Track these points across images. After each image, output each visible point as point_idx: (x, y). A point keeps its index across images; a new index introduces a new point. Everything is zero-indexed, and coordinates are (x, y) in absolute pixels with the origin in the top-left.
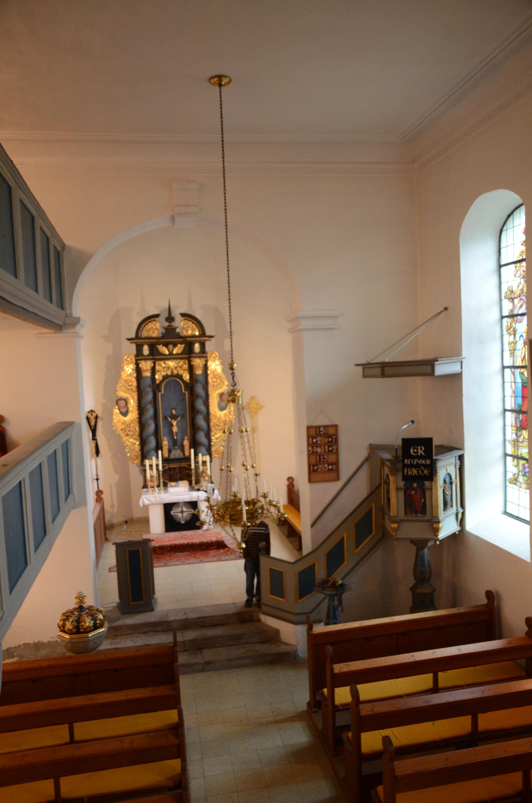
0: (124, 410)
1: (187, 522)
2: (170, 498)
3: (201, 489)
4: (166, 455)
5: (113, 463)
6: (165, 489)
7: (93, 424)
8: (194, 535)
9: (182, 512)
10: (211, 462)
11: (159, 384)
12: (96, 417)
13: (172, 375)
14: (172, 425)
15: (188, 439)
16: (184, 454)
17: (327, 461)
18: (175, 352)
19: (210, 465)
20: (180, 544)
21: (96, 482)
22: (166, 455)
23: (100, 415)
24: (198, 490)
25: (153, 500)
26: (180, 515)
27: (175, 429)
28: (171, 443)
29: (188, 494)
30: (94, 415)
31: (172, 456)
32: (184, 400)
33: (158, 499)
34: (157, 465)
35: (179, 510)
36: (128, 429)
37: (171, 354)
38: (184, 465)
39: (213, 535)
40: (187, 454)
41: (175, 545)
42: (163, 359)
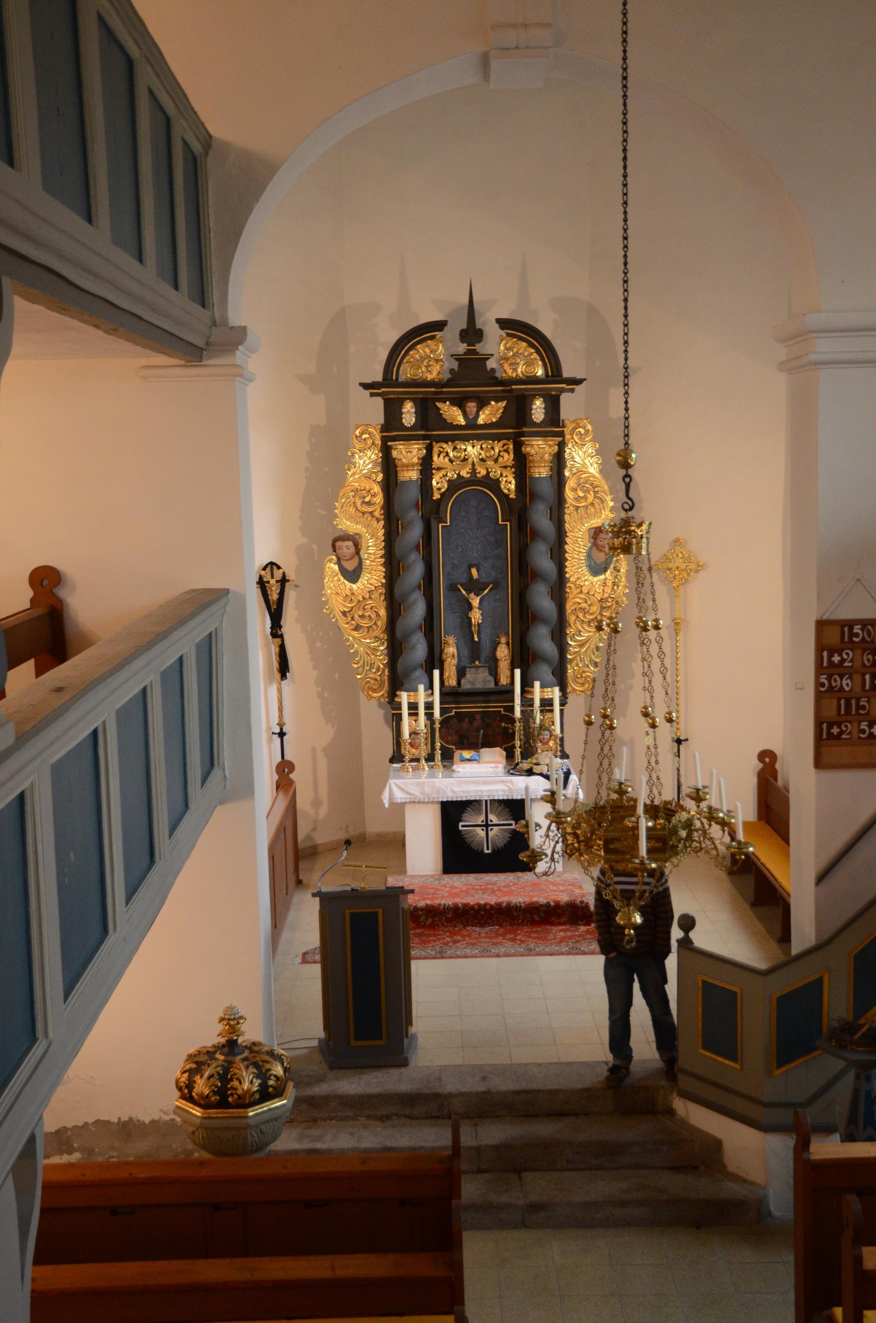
0: (350, 566)
1: (497, 852)
2: (456, 789)
3: (536, 769)
5: (320, 695)
8: (515, 884)
9: (487, 825)
10: (563, 704)
12: (283, 581)
13: (474, 480)
15: (508, 644)
16: (497, 683)
17: (868, 713)
19: (562, 711)
20: (479, 905)
21: (277, 740)
22: (452, 682)
23: (291, 575)
24: (530, 772)
25: (417, 793)
26: (481, 832)
27: (476, 616)
28: (466, 653)
29: (503, 782)
30: (278, 574)
31: (466, 685)
32: (500, 543)
33: (427, 790)
36: (360, 613)
39: (561, 888)
40: (504, 680)
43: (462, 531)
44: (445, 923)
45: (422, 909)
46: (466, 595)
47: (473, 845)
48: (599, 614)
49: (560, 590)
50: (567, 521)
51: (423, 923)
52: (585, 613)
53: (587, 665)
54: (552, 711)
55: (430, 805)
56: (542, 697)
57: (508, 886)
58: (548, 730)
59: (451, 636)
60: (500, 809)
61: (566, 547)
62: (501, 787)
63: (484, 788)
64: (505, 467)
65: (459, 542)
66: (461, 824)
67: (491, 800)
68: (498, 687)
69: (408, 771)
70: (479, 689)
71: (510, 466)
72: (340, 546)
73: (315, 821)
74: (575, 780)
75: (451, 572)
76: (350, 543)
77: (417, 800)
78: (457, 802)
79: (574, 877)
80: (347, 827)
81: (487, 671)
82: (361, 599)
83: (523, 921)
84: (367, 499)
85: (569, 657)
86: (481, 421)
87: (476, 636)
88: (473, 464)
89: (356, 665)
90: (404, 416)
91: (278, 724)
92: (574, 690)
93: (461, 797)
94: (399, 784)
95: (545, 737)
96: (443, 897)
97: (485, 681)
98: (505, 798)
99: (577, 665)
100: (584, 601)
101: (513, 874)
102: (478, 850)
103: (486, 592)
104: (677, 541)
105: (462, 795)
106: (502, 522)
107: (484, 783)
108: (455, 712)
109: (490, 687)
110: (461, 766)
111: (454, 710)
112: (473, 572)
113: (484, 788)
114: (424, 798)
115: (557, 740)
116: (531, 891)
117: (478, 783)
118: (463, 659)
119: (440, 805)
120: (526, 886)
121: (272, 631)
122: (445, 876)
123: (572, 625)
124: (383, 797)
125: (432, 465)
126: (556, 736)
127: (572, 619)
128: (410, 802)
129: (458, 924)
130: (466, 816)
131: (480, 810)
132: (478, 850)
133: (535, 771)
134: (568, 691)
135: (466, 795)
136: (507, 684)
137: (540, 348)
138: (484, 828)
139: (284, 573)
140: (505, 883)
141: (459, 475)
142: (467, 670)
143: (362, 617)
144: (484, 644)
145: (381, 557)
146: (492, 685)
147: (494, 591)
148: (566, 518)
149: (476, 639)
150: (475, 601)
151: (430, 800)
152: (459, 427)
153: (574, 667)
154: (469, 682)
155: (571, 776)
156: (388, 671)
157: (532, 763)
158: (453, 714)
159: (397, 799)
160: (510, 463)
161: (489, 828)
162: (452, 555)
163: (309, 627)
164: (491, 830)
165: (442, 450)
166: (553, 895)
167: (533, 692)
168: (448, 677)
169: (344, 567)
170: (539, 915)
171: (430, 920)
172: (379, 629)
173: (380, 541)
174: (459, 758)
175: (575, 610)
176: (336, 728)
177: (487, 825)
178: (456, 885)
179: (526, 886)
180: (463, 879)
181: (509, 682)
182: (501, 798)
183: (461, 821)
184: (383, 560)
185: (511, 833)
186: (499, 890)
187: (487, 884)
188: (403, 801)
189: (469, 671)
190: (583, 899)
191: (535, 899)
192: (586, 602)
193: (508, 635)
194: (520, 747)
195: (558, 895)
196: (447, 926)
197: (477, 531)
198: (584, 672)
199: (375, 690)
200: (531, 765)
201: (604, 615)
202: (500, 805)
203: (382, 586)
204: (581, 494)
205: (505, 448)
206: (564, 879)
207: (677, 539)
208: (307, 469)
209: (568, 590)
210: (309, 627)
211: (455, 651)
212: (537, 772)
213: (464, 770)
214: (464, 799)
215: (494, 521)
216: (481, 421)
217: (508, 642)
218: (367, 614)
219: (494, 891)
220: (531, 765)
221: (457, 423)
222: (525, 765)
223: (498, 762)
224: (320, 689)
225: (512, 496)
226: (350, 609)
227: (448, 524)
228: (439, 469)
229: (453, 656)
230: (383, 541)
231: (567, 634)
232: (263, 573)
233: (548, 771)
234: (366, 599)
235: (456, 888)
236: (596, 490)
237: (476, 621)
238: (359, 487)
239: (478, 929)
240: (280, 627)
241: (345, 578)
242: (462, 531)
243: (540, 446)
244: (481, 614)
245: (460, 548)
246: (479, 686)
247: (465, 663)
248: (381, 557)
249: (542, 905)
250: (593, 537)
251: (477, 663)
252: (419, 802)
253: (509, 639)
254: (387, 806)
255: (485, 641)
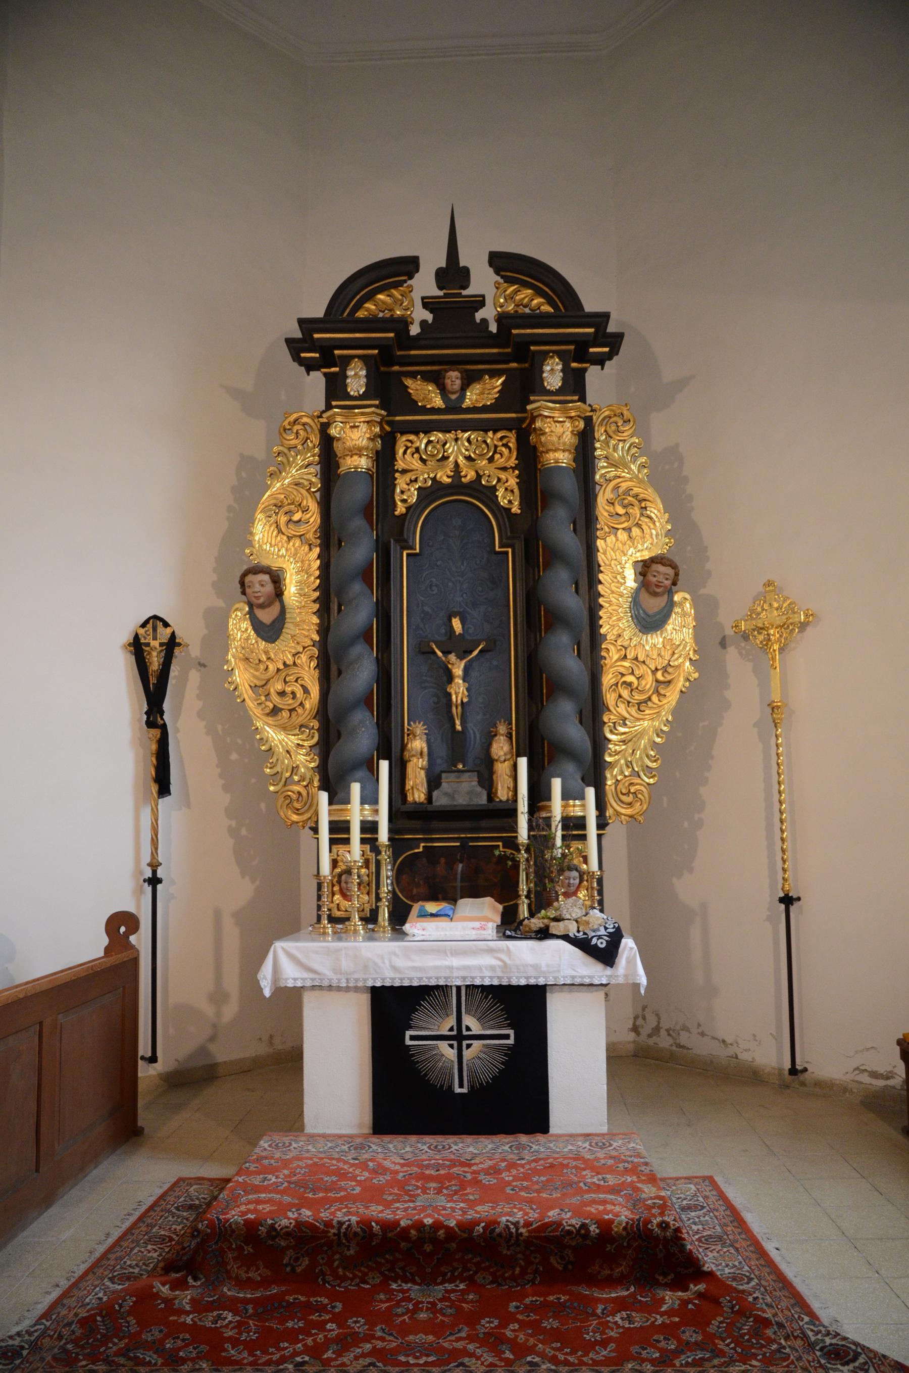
0: (267, 616)
1: (479, 1092)
2: (400, 963)
3: (556, 928)
4: (417, 793)
5: (233, 832)
6: (394, 930)
7: (155, 662)
8: (512, 1165)
9: (459, 1037)
10: (602, 824)
11: (403, 517)
12: (172, 644)
13: (457, 486)
14: (450, 678)
15: (509, 736)
16: (490, 798)
18: (472, 397)
19: (599, 836)
20: (419, 1226)
21: (148, 889)
22: (417, 793)
23: (181, 636)
24: (544, 934)
25: (326, 970)
26: (448, 1051)
27: (459, 690)
28: (442, 751)
29: (491, 951)
30: (164, 634)
31: (441, 800)
32: (499, 581)
33: (346, 964)
34: (369, 828)
35: (447, 1025)
36: (279, 687)
37: (453, 407)
38: (484, 839)
39: (612, 1180)
40: (503, 794)
41: (389, 1226)
42: (426, 428)
43: (439, 563)
44: (340, 1271)
45: (287, 1234)
46: (444, 659)
47: (432, 1077)
48: (653, 693)
49: (592, 652)
50: (600, 549)
51: (288, 1269)
52: (632, 690)
53: (638, 772)
54: (583, 838)
55: (352, 995)
56: (565, 815)
57: (494, 1171)
58: (577, 870)
59: (419, 723)
60: (485, 1005)
61: (600, 587)
62: (488, 961)
63: (455, 962)
64: (504, 469)
65: (434, 580)
66: (408, 1033)
67: (467, 986)
68: (494, 804)
69: (324, 934)
70: (464, 805)
71: (511, 467)
72: (251, 582)
73: (214, 1026)
74: (631, 949)
75: (421, 626)
76: (266, 578)
77: (326, 983)
78: (402, 988)
79: (634, 1149)
80: (271, 1037)
81: (476, 779)
82: (282, 667)
83: (524, 1272)
84: (296, 517)
85: (608, 759)
86: (467, 403)
87: (458, 722)
88: (456, 464)
89: (268, 770)
90: (348, 381)
91: (149, 865)
92: (618, 814)
93: (411, 979)
94: (285, 947)
95: (572, 881)
96: (350, 1198)
97: (470, 793)
98: (496, 982)
99: (622, 772)
100: (631, 671)
101: (510, 1138)
102: (442, 1086)
103: (475, 653)
104: (769, 583)
105: (413, 974)
106: (499, 548)
107: (455, 953)
108: (423, 847)
109: (480, 803)
110: (418, 925)
111: (422, 844)
112: (454, 624)
113: (455, 962)
114: (339, 980)
115: (592, 883)
116: (545, 1187)
117: (442, 952)
118: (439, 761)
119: (369, 995)
120: (536, 1172)
121: (148, 718)
122: (375, 1139)
123: (612, 708)
124: (260, 976)
125: (395, 465)
126: (591, 874)
127: (610, 698)
128: (313, 987)
129: (370, 1275)
130: (418, 1017)
131: (445, 1006)
132: (442, 1086)
133: (553, 931)
134: (607, 815)
135: (419, 975)
136: (508, 800)
137: (554, 297)
138: (455, 1043)
139: (173, 632)
140: (490, 1163)
141: (434, 479)
142: (444, 775)
143: (282, 694)
144: (472, 743)
145: (314, 601)
146: (483, 800)
147: (488, 655)
148: (599, 559)
149: (459, 728)
150: (458, 670)
151: (351, 985)
152: (434, 411)
153: (616, 776)
154: (446, 794)
155: (623, 941)
156: (320, 780)
157: (549, 918)
158: (421, 850)
159: (288, 979)
160: (513, 462)
161: (465, 1043)
162: (423, 599)
163: (220, 727)
164: (469, 1046)
165: (409, 444)
166: (594, 1202)
167: (550, 806)
168: (412, 788)
169: (258, 618)
170: (562, 1258)
171: (306, 1262)
172: (307, 712)
173: (313, 578)
174: (417, 911)
175: (617, 684)
176: (258, 883)
177: (459, 1037)
178: (387, 1164)
179: (536, 1172)
180: (408, 1149)
181: (510, 798)
182: (487, 982)
183: (410, 1027)
184: (316, 606)
185: (506, 1055)
186: (476, 1182)
187: (454, 1163)
188: (299, 984)
189: (447, 778)
190: (666, 1218)
191: (553, 1214)
192: (632, 673)
193: (510, 723)
194: (528, 897)
195: (604, 1202)
196: (343, 1279)
197: (463, 564)
198: (631, 784)
199: (298, 810)
200: (546, 921)
201: (661, 694)
202: (486, 997)
203: (313, 646)
204: (621, 511)
205: (504, 442)
206: (614, 1153)
207: (769, 581)
208: (230, 509)
209: (603, 654)
210: (220, 727)
211: (424, 745)
212: (559, 934)
213: (423, 933)
214: (415, 984)
215: (488, 549)
216: (467, 403)
217: (511, 734)
218: (288, 689)
219: (463, 1185)
220: (546, 921)
221: (433, 405)
222: (536, 923)
223: (488, 920)
224: (233, 823)
225: (515, 509)
226: (265, 682)
227: (418, 551)
228: (404, 472)
229: (421, 754)
230: (317, 578)
231: (605, 723)
232: (141, 631)
233: (578, 931)
234: (288, 666)
235: (385, 1170)
236: (643, 505)
237: (459, 699)
238: (285, 500)
239: (414, 1291)
240: (162, 713)
241: (254, 629)
242: (439, 563)
243: (556, 419)
244: (468, 690)
245: (434, 588)
246: (462, 801)
247: (441, 765)
248: (314, 601)
249: (569, 1233)
250: (640, 574)
251: (460, 766)
252: (330, 988)
253: (511, 729)
254: (267, 993)
255: (474, 733)
